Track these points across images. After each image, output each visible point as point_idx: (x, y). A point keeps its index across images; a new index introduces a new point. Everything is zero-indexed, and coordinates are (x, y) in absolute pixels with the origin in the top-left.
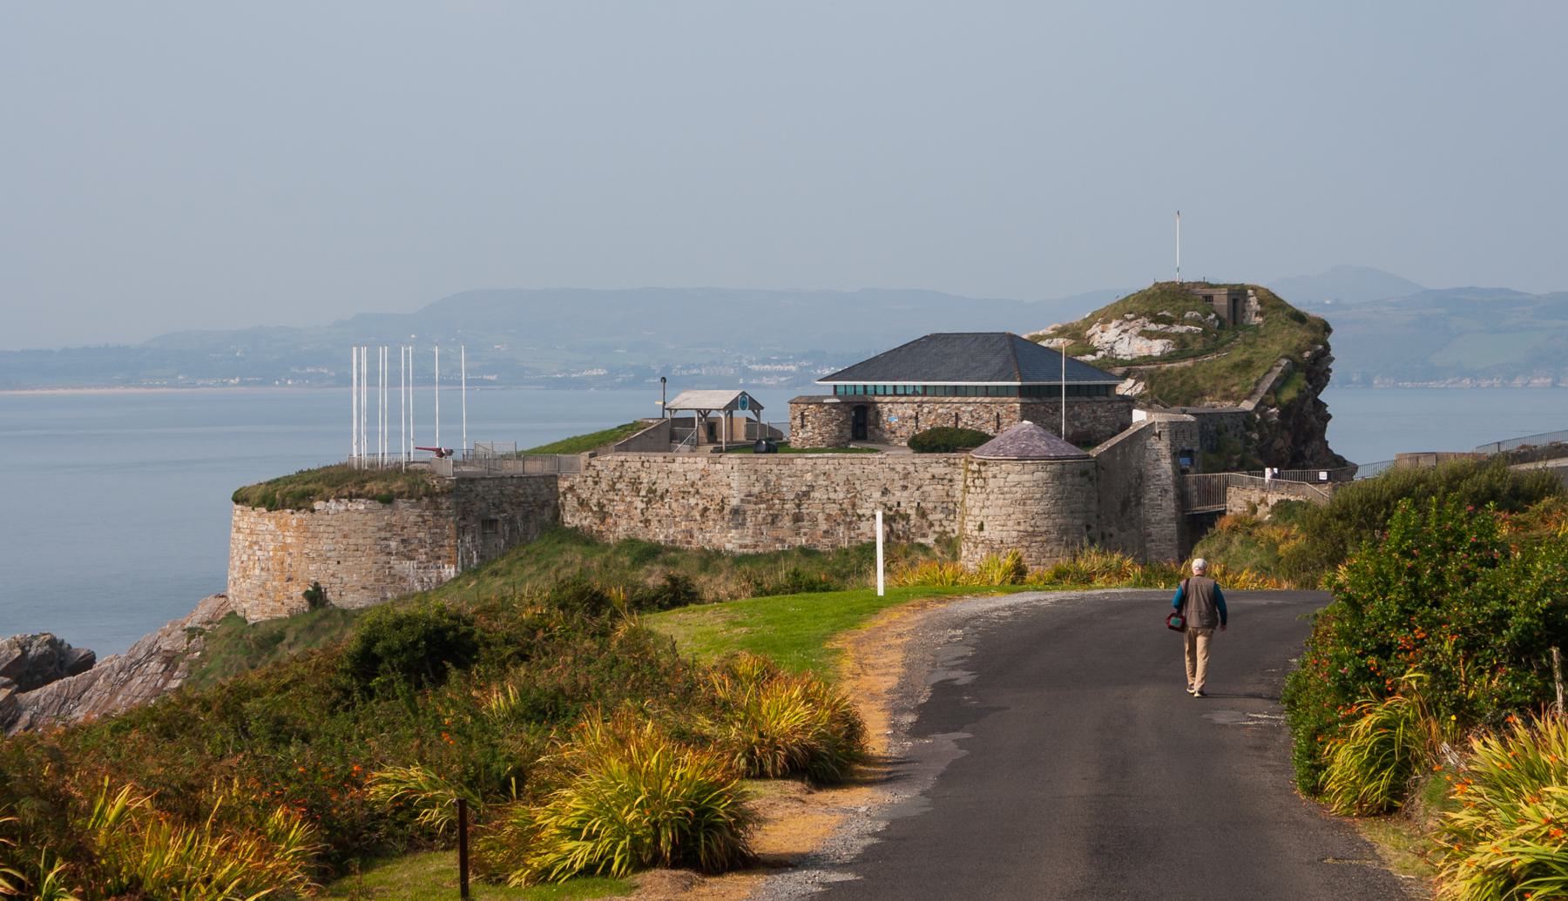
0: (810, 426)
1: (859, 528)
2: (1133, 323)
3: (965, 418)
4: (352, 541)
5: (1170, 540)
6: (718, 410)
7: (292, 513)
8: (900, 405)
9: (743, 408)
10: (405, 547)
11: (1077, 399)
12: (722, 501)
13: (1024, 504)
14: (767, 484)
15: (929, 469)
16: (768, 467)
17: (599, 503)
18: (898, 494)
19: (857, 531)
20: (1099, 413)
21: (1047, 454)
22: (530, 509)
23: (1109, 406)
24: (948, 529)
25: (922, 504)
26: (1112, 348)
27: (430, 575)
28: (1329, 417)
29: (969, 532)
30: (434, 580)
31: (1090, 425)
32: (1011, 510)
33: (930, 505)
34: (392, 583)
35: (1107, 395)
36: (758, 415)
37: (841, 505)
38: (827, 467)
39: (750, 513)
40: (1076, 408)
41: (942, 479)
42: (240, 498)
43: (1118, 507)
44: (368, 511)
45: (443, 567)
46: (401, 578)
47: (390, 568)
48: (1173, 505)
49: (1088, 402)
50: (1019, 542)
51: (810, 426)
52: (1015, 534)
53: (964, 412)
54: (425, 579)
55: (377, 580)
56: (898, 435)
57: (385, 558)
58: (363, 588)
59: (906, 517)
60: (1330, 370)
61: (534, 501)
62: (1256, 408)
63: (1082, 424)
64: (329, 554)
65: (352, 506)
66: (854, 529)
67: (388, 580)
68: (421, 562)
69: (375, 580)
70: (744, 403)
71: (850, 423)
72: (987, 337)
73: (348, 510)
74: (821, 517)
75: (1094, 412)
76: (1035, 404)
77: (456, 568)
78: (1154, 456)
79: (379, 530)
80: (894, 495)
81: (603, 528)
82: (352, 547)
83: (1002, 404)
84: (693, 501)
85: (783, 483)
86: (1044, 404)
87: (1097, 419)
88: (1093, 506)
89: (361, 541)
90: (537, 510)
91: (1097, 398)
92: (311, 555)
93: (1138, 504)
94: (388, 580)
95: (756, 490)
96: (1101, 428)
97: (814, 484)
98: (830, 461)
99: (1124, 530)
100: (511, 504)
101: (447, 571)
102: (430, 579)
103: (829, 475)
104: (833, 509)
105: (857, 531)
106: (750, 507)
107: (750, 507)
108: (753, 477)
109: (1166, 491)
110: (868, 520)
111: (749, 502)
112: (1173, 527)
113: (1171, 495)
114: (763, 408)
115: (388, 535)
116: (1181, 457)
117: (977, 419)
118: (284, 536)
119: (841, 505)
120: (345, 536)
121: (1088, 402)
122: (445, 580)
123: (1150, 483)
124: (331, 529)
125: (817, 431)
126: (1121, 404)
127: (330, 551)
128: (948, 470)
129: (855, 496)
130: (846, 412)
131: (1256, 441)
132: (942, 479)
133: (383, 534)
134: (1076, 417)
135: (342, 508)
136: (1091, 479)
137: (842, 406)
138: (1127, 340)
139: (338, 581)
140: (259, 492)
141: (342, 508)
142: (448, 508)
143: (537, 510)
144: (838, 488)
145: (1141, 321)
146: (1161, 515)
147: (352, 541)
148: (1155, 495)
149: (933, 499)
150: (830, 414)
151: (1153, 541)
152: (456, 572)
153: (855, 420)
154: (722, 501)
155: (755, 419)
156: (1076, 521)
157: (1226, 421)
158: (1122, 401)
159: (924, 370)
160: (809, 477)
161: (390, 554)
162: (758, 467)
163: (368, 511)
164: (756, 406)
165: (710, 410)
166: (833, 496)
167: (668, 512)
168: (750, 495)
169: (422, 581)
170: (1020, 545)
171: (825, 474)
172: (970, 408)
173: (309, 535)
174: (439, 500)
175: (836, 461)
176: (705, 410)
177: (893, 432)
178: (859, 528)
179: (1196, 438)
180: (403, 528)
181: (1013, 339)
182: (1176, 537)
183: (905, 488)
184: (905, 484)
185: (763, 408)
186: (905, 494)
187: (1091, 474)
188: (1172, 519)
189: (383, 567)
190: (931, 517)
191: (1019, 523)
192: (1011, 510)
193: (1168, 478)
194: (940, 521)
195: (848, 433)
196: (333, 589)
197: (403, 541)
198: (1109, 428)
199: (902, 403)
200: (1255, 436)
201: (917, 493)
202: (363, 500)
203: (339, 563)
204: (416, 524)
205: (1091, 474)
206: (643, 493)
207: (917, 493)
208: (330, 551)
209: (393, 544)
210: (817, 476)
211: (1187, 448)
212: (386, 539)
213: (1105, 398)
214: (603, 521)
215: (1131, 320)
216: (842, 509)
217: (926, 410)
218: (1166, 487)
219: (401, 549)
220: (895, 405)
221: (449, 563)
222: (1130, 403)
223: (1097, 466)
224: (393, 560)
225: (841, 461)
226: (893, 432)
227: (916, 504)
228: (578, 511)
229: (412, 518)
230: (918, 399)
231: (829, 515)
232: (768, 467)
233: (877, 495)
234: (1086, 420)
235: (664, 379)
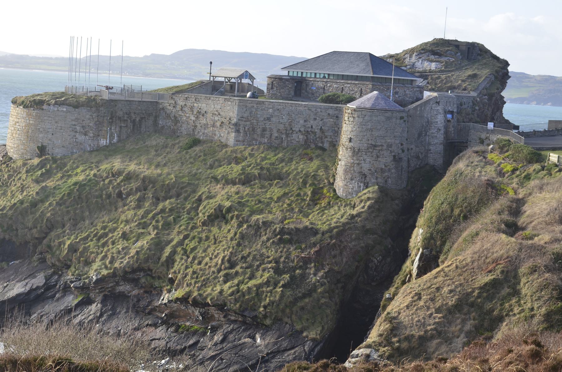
0: (275, 89)
1: (292, 137)
2: (423, 55)
3: (346, 90)
4: (59, 125)
5: (440, 153)
6: (234, 78)
7: (34, 110)
8: (317, 82)
9: (246, 78)
10: (83, 129)
11: (398, 85)
12: (230, 119)
13: (372, 131)
14: (251, 113)
15: (327, 111)
16: (252, 105)
17: (175, 116)
18: (312, 122)
19: (291, 138)
20: (407, 92)
21: (385, 108)
22: (144, 116)
23: (412, 89)
24: (334, 140)
25: (323, 128)
26: (414, 65)
27: (95, 143)
28: (505, 103)
29: (344, 143)
30: (96, 146)
31: (402, 97)
32: (365, 133)
33: (327, 128)
34: (76, 145)
35: (412, 84)
36: (253, 82)
37: (284, 125)
38: (279, 107)
39: (242, 126)
40: (397, 89)
41: (333, 116)
42: (14, 102)
43: (416, 136)
44: (67, 112)
45: (101, 140)
46: (80, 144)
47: (76, 138)
48: (442, 137)
49: (402, 87)
50: (368, 149)
51: (275, 89)
52: (366, 145)
53: (346, 87)
54: (92, 145)
55: (70, 144)
56: (315, 95)
57: (73, 134)
58: (63, 147)
59: (315, 133)
60: (507, 83)
61: (145, 113)
62: (478, 96)
63: (399, 97)
64: (48, 130)
65: (61, 109)
66: (290, 137)
67: (75, 144)
68: (90, 137)
69: (69, 144)
70: (246, 76)
71: (294, 88)
72: (359, 54)
73: (58, 110)
74: (275, 131)
75: (405, 91)
76: (379, 85)
77: (106, 141)
78: (435, 113)
79: (72, 120)
80: (310, 122)
81: (175, 128)
82: (60, 128)
83: (363, 84)
84: (216, 118)
85: (258, 113)
86: (383, 85)
87: (406, 95)
88: (405, 135)
89: (63, 125)
90: (146, 117)
91: (407, 85)
92: (41, 130)
93: (426, 135)
94: (75, 144)
95: (245, 115)
96: (407, 99)
97: (273, 114)
98: (281, 104)
99: (418, 147)
100: (135, 113)
101: (102, 142)
102: (94, 145)
103: (280, 110)
104: (281, 127)
105: (291, 138)
106: (242, 123)
107: (242, 123)
108: (245, 109)
109: (440, 130)
110: (297, 133)
111: (242, 121)
112: (441, 147)
113: (442, 132)
114: (255, 79)
115: (76, 123)
116: (316, 150)
117: (352, 91)
118: (29, 120)
119: (284, 125)
120: (56, 122)
121: (402, 87)
122: (101, 146)
123: (432, 125)
124: (50, 119)
125: (278, 91)
126: (417, 89)
127: (49, 129)
128: (336, 112)
129: (291, 122)
130: (292, 83)
131: (477, 110)
132: (333, 116)
133: (74, 123)
134: (396, 93)
135: (56, 109)
136: (405, 121)
137: (290, 80)
138: (420, 61)
139: (52, 143)
140: (22, 99)
141: (56, 109)
142: (105, 113)
143: (146, 117)
144: (284, 117)
145: (427, 54)
146: (436, 141)
147: (59, 125)
148: (434, 131)
149: (328, 125)
150: (285, 84)
151: (431, 153)
152: (106, 143)
153: (296, 87)
154: (230, 119)
155: (251, 84)
156: (396, 141)
157: (465, 100)
158: (418, 88)
159: (329, 67)
160: (271, 110)
161: (76, 132)
162: (248, 105)
163: (67, 112)
164: (252, 78)
165: (232, 78)
166: (281, 121)
167: (205, 122)
168: (243, 117)
169: (91, 146)
170: (368, 151)
171: (278, 110)
172: (349, 85)
173: (40, 120)
174: (101, 109)
175: (284, 104)
176: (229, 78)
177: (313, 94)
178: (292, 137)
179: (455, 106)
180: (83, 120)
181: (371, 55)
182: (442, 152)
183: (315, 119)
184: (316, 117)
185: (255, 79)
186: (316, 122)
187: (405, 119)
188: (441, 143)
189: (73, 138)
190: (326, 134)
191: (368, 140)
192: (365, 133)
193: (441, 123)
194: (331, 136)
195: (292, 93)
196: (50, 146)
197: (83, 127)
198: (411, 99)
199: (318, 81)
200: (477, 108)
201: (321, 122)
202: (65, 106)
203: (53, 134)
204: (89, 119)
205: (405, 119)
206: (195, 113)
207: (321, 122)
208: (49, 129)
209: (78, 128)
210: (274, 110)
211: (451, 110)
212: (75, 125)
213: (410, 86)
214: (176, 124)
215: (423, 53)
216: (285, 127)
217: (329, 85)
218: (440, 128)
219: (82, 130)
220: (315, 82)
221: (103, 138)
222: (421, 90)
223: (408, 115)
224: (77, 135)
225: (286, 105)
226: (313, 94)
227: (320, 127)
228: (165, 119)
229: (88, 116)
230: (325, 80)
231: (279, 129)
232: (252, 105)
233: (302, 122)
234: (401, 95)
235: (211, 63)
